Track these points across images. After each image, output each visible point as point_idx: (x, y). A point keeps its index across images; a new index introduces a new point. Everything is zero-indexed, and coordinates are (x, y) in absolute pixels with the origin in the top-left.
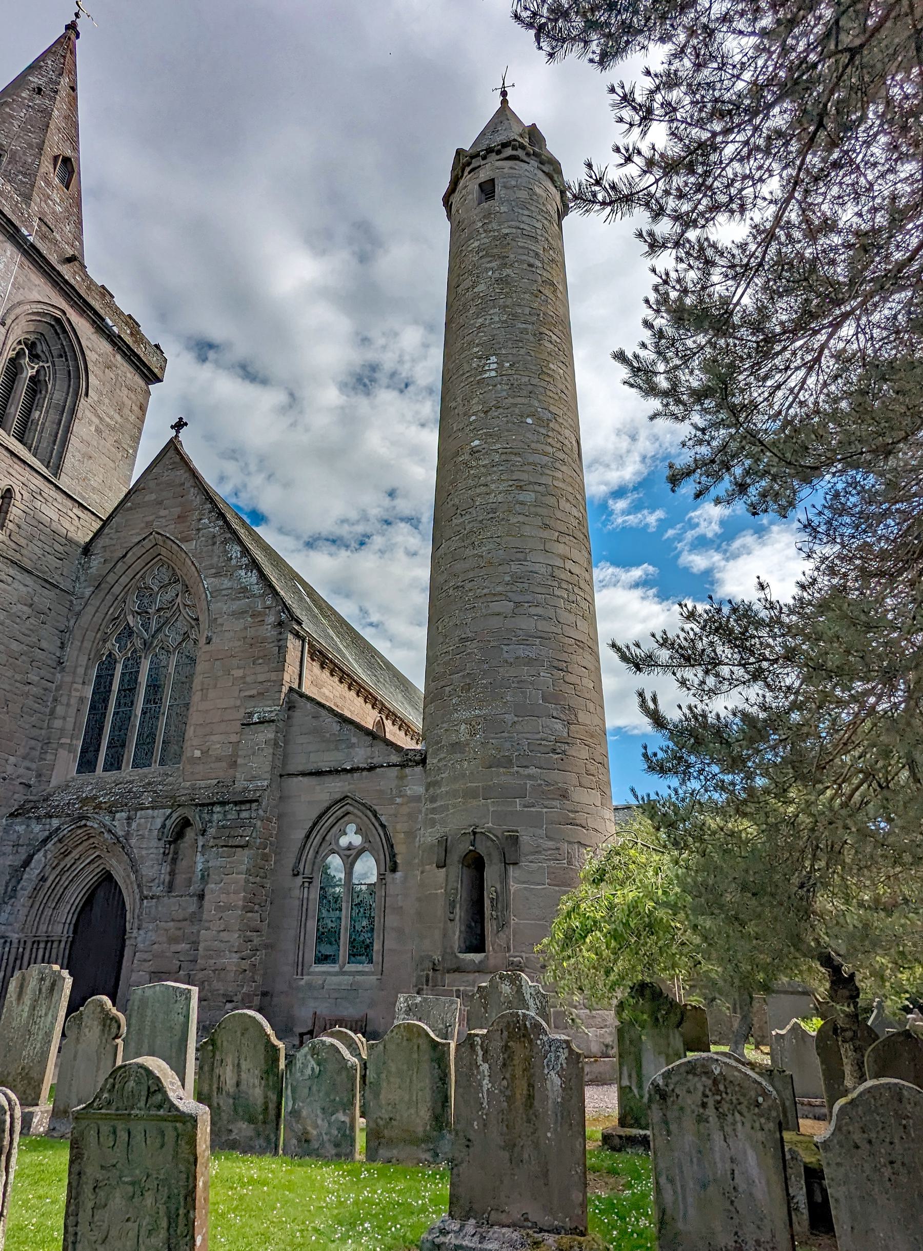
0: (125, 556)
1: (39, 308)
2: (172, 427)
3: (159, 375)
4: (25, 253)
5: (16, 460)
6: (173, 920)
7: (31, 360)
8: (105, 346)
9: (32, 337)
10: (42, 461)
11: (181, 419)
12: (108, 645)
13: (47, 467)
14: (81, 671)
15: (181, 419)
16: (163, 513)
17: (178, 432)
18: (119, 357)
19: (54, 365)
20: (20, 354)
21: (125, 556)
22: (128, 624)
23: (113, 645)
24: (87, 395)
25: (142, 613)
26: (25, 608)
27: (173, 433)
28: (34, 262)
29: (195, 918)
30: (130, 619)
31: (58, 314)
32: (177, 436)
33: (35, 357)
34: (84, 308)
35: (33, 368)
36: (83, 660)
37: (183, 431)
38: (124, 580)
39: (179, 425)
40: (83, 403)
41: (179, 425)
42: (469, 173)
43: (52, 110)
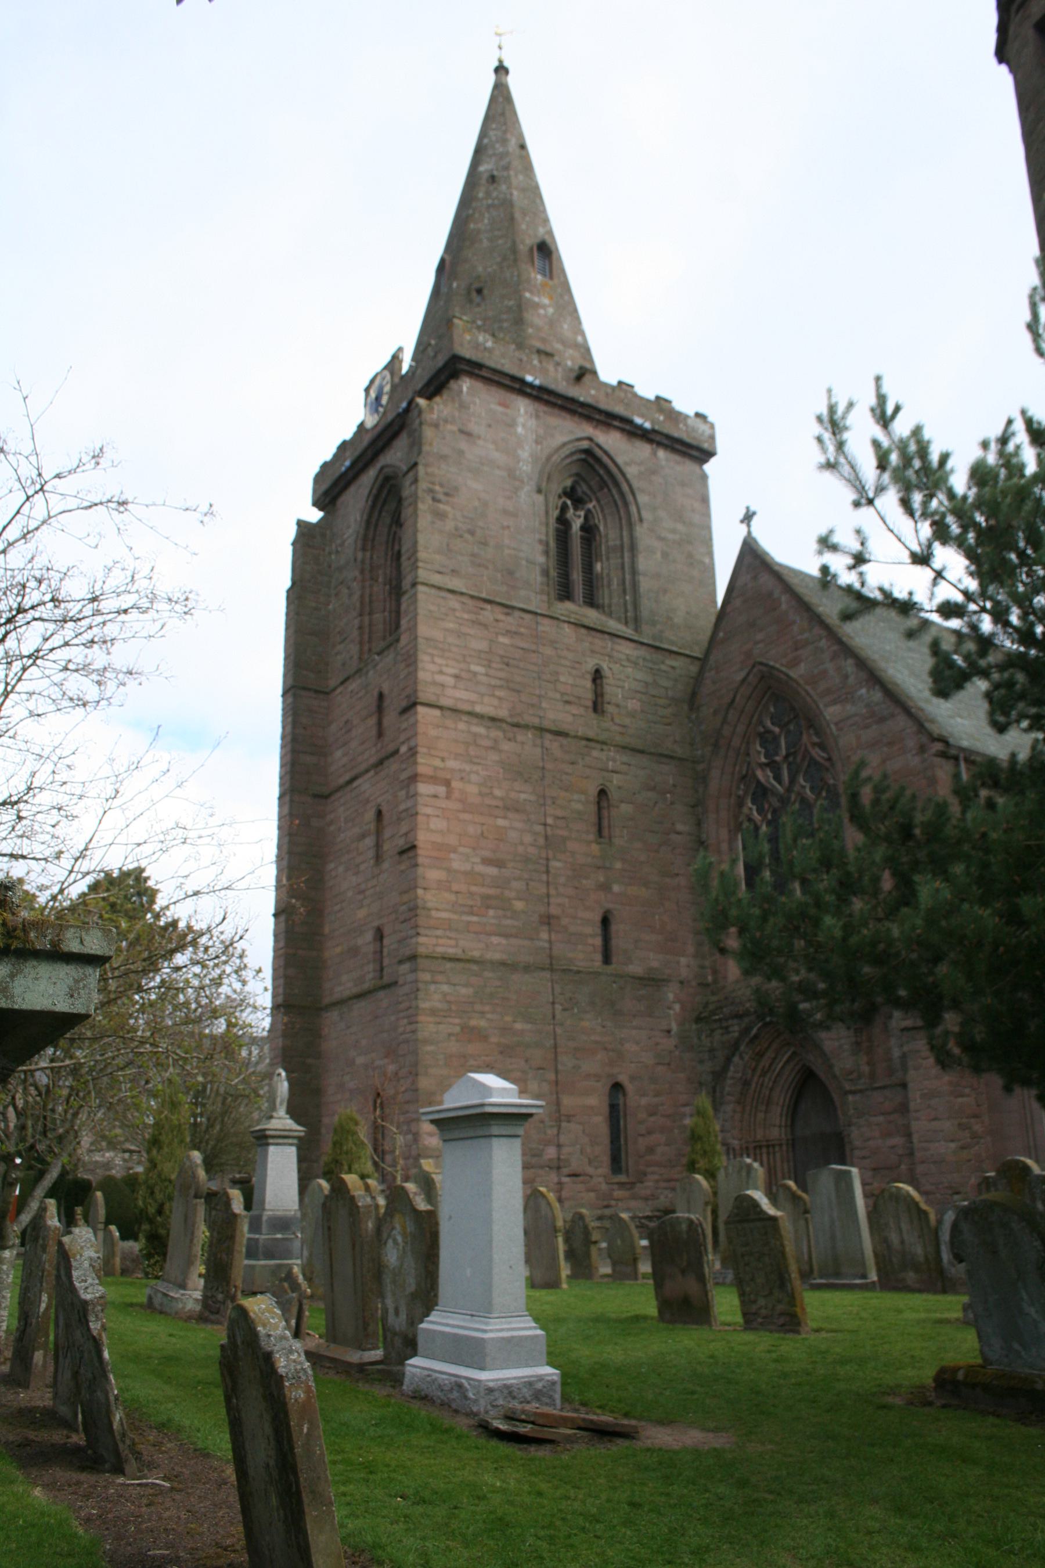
0: (733, 701)
1: (566, 451)
2: (742, 522)
3: (710, 449)
4: (537, 399)
5: (593, 633)
6: (883, 1114)
7: (576, 509)
8: (643, 450)
9: (569, 483)
10: (619, 620)
11: (748, 508)
12: (745, 810)
13: (626, 623)
14: (724, 846)
15: (748, 508)
16: (759, 636)
17: (749, 526)
18: (661, 453)
19: (598, 501)
20: (564, 509)
21: (733, 701)
22: (758, 782)
23: (751, 809)
24: (641, 520)
25: (772, 765)
26: (650, 794)
27: (744, 527)
28: (547, 403)
29: (903, 1108)
30: (759, 774)
31: (585, 444)
32: (749, 533)
33: (578, 502)
34: (607, 419)
35: (579, 517)
36: (724, 834)
37: (754, 522)
38: (741, 729)
39: (748, 517)
40: (640, 531)
41: (748, 517)
42: (1018, 11)
43: (511, 194)
